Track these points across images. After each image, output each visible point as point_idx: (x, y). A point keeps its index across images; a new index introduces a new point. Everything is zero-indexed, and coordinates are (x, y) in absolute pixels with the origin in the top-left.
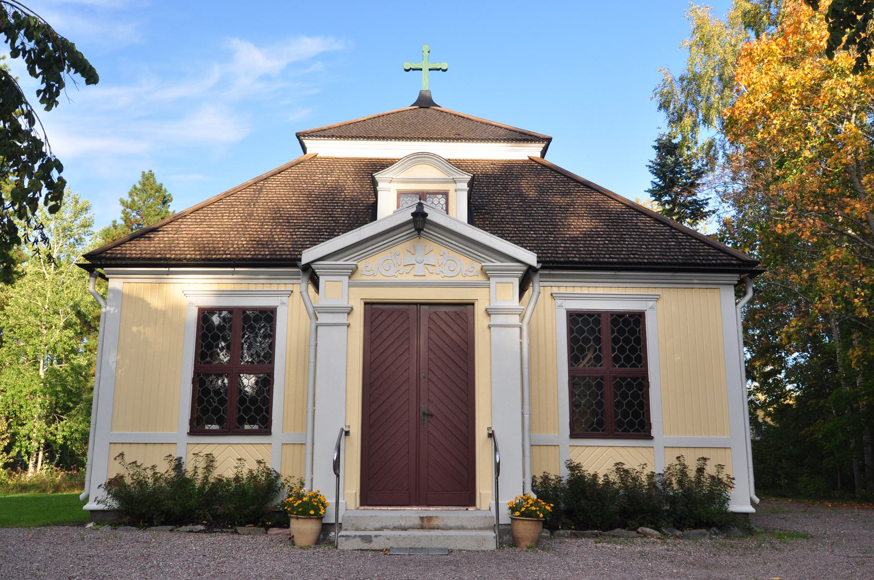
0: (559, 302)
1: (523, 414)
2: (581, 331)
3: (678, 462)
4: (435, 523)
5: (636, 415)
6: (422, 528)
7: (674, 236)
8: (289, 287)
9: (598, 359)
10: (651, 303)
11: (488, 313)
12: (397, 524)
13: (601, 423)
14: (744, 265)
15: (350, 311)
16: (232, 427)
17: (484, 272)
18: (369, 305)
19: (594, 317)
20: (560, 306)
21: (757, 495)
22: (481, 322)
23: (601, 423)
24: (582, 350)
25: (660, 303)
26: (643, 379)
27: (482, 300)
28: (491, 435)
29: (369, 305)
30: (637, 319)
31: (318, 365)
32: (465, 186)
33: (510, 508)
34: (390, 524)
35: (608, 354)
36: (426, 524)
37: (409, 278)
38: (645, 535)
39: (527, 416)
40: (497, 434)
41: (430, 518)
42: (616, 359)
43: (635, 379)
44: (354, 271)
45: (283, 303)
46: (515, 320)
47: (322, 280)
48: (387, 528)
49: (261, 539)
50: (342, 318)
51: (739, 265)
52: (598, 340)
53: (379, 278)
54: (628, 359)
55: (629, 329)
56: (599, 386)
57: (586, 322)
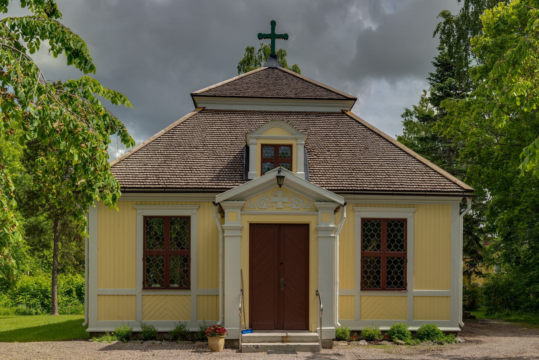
4: (289, 339)
5: (399, 278)
6: (282, 342)
9: (378, 246)
12: (270, 340)
13: (396, 225)
14: (466, 192)
15: (241, 229)
16: (169, 220)
18: (252, 226)
19: (378, 222)
21: (463, 321)
23: (378, 283)
28: (317, 294)
35: (384, 244)
36: (285, 339)
37: (274, 211)
38: (398, 344)
41: (287, 337)
42: (389, 247)
43: (399, 258)
47: (226, 211)
48: (265, 349)
50: (238, 233)
51: (462, 192)
52: (379, 236)
54: (396, 247)
56: (379, 262)
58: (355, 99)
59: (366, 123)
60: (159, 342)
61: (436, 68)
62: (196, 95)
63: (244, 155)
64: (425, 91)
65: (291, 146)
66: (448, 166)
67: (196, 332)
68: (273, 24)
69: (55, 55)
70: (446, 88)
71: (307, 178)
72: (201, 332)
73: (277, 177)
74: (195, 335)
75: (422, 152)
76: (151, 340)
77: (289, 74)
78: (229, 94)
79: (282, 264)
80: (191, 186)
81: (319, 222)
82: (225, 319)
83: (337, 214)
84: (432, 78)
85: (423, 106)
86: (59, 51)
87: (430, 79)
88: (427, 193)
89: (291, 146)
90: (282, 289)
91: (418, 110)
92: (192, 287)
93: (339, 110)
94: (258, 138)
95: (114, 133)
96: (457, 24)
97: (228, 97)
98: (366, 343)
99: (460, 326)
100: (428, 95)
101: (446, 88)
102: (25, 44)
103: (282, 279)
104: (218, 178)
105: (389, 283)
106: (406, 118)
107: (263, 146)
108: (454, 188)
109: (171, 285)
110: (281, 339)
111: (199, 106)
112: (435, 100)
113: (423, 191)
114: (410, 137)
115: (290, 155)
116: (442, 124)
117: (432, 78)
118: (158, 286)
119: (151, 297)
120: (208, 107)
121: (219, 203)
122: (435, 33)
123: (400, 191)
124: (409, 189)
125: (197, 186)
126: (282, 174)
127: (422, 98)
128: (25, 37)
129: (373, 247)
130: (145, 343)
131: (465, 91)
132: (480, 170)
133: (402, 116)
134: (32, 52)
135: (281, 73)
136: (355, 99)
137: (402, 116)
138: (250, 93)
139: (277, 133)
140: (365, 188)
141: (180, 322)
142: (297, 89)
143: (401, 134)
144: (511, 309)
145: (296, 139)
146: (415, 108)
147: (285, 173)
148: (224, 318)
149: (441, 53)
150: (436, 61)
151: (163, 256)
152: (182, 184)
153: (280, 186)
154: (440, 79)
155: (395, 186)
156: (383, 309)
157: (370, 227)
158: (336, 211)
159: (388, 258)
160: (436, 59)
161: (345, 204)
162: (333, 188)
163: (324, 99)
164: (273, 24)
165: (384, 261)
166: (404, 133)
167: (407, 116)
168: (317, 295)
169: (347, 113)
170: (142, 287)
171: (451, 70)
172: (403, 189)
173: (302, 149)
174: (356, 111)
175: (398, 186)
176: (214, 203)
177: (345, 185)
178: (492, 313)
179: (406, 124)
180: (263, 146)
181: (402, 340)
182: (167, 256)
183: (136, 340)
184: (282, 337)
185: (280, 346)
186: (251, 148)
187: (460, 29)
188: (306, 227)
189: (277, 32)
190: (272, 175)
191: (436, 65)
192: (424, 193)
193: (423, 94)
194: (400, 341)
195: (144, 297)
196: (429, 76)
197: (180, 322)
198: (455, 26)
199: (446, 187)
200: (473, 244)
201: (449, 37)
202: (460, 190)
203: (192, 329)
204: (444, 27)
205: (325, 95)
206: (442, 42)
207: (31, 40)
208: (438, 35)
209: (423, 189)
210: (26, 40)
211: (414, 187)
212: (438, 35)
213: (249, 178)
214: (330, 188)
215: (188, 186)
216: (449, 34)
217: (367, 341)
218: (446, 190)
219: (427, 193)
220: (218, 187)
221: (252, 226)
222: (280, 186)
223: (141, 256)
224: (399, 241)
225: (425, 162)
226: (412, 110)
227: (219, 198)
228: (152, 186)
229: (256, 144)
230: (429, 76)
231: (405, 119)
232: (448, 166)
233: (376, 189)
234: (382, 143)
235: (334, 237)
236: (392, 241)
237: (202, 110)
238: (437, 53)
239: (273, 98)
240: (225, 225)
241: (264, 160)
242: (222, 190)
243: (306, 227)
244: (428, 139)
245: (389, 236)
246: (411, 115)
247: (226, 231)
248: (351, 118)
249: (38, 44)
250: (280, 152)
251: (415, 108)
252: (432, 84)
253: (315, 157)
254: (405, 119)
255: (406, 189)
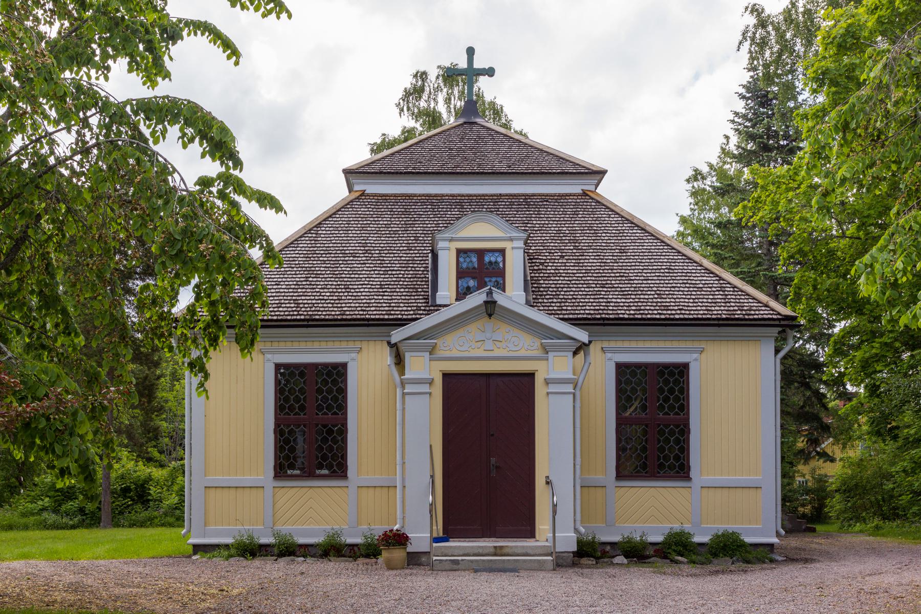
0: (609, 355)
1: (575, 521)
2: (628, 382)
3: (890, 446)
4: (505, 551)
6: (495, 555)
7: (722, 289)
8: (358, 345)
10: (695, 356)
11: (547, 382)
12: (476, 551)
13: (644, 467)
15: (431, 382)
17: (546, 350)
20: (610, 359)
22: (540, 390)
24: (629, 399)
25: (703, 355)
26: (685, 427)
27: (542, 371)
29: (447, 376)
30: (682, 370)
31: (407, 426)
32: (521, 244)
33: (580, 543)
34: (471, 551)
36: (498, 551)
38: (677, 562)
39: (578, 467)
40: (554, 482)
41: (501, 547)
43: (677, 426)
44: (432, 350)
45: (353, 359)
46: (569, 388)
49: (350, 565)
50: (425, 388)
51: (778, 319)
53: (455, 353)
55: (674, 379)
57: (634, 374)
59: (623, 210)
60: (302, 559)
61: (742, 103)
63: (430, 266)
64: (727, 137)
65: (502, 251)
66: (765, 270)
67: (357, 545)
68: (471, 52)
69: (185, 146)
70: (761, 137)
71: (527, 302)
72: (364, 545)
73: (486, 302)
74: (356, 549)
75: (722, 246)
76: (289, 555)
77: (497, 132)
78: (403, 170)
79: (493, 435)
80: (349, 317)
81: (554, 368)
82: (407, 520)
83: (578, 356)
84: (736, 119)
85: (724, 163)
86: (191, 140)
87: (733, 121)
88: (721, 322)
89: (502, 251)
90: (494, 474)
91: (715, 170)
94: (451, 240)
95: (254, 247)
96: (777, 29)
97: (401, 173)
98: (625, 561)
100: (732, 147)
101: (761, 137)
102: (146, 132)
103: (493, 460)
106: (695, 184)
107: (460, 252)
108: (764, 313)
109: (318, 472)
110: (492, 550)
111: (356, 188)
112: (745, 158)
113: (714, 319)
114: (702, 216)
115: (501, 265)
116: (750, 205)
117: (736, 119)
118: (298, 472)
119: (287, 489)
121: (396, 344)
122: (740, 43)
123: (677, 319)
124: (691, 317)
125: (359, 317)
127: (723, 150)
128: (148, 122)
129: (636, 409)
130: (279, 560)
131: (795, 141)
132: (815, 280)
133: (688, 181)
134: (156, 142)
135: (483, 132)
136: (603, 173)
137: (688, 181)
138: (435, 166)
139: (481, 231)
140: (621, 316)
141: (333, 529)
142: (509, 158)
143: (686, 212)
144: (885, 518)
145: (511, 239)
146: (711, 166)
147: (498, 296)
149: (752, 77)
150: (743, 91)
151: (305, 426)
152: (335, 313)
154: (750, 120)
155: (669, 312)
158: (575, 353)
159: (659, 425)
160: (744, 86)
161: (590, 342)
162: (571, 316)
163: (554, 173)
164: (471, 52)
165: (653, 428)
166: (691, 209)
167: (696, 179)
168: (547, 483)
171: (770, 105)
172: (682, 316)
173: (520, 254)
174: (606, 190)
175: (673, 312)
176: (389, 343)
177: (587, 311)
178: (850, 526)
179: (694, 194)
180: (460, 252)
181: (682, 556)
182: (311, 428)
183: (267, 555)
184: (495, 547)
185: (491, 560)
186: (442, 255)
187: (781, 36)
188: (530, 376)
189: (477, 65)
190: (477, 299)
191: (743, 97)
192: (716, 322)
193: (725, 141)
194: (680, 558)
195: (277, 489)
196: (731, 117)
197: (333, 529)
198: (773, 33)
199: (753, 312)
200: (812, 405)
201: (762, 51)
202: (775, 317)
203: (350, 541)
204: (754, 33)
205: (556, 167)
206: (752, 59)
207: (155, 127)
208: (747, 44)
209: (714, 317)
210: (149, 127)
211: (701, 313)
212: (747, 44)
214: (566, 316)
215: (344, 317)
216: (763, 44)
217: (626, 557)
218: (751, 317)
219: (721, 322)
220: (391, 317)
221: (447, 377)
223: (272, 427)
224: (677, 399)
225: (718, 273)
226: (705, 169)
227: (397, 335)
228: (289, 318)
229: (448, 249)
230: (731, 117)
231: (693, 187)
232: (765, 270)
233: (640, 316)
234: (648, 242)
237: (361, 195)
238: (746, 77)
239: (474, 173)
240: (406, 376)
241: (461, 274)
242: (400, 323)
243: (530, 376)
244: (732, 224)
246: (704, 178)
247: (407, 386)
249: (164, 132)
250: (487, 259)
251: (711, 166)
252: (736, 130)
253: (541, 267)
254: (693, 187)
255: (686, 316)
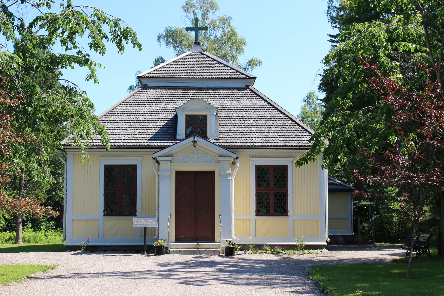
4: (201, 246)
58: (255, 78)
62: (140, 77)
92: (137, 214)
93: (244, 85)
99: (327, 241)
104: (154, 138)
105: (275, 211)
111: (143, 84)
120: (149, 84)
126: (195, 140)
136: (255, 78)
148: (159, 233)
153: (195, 147)
156: (271, 229)
157: (261, 171)
169: (250, 87)
170: (102, 214)
186: (179, 117)
213: (178, 137)
221: (178, 173)
222: (195, 147)
235: (230, 179)
236: (278, 181)
245: (275, 177)
248: (253, 92)
